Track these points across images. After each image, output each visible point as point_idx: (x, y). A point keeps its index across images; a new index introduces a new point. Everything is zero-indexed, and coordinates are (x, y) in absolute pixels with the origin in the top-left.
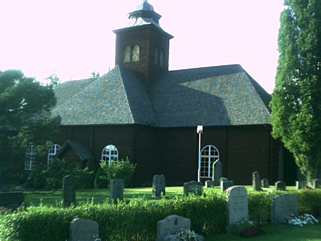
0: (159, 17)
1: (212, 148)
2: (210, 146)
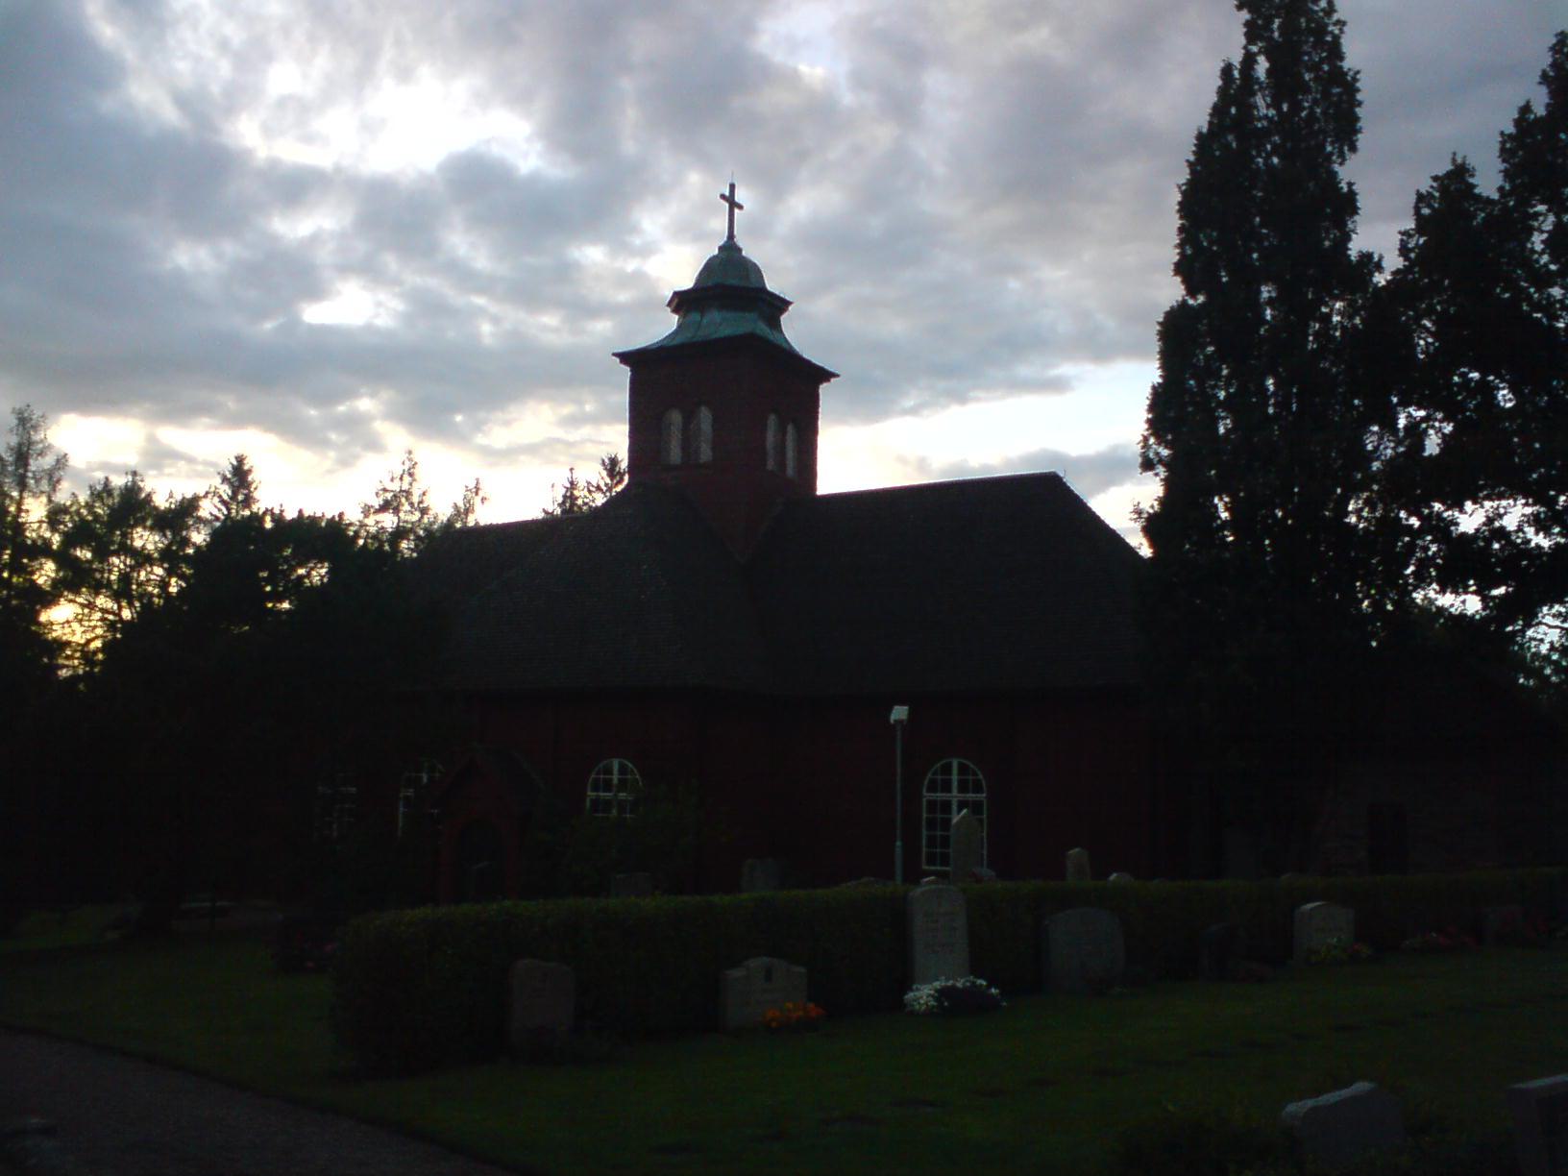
0: (780, 305)
1: (963, 769)
2: (616, 764)
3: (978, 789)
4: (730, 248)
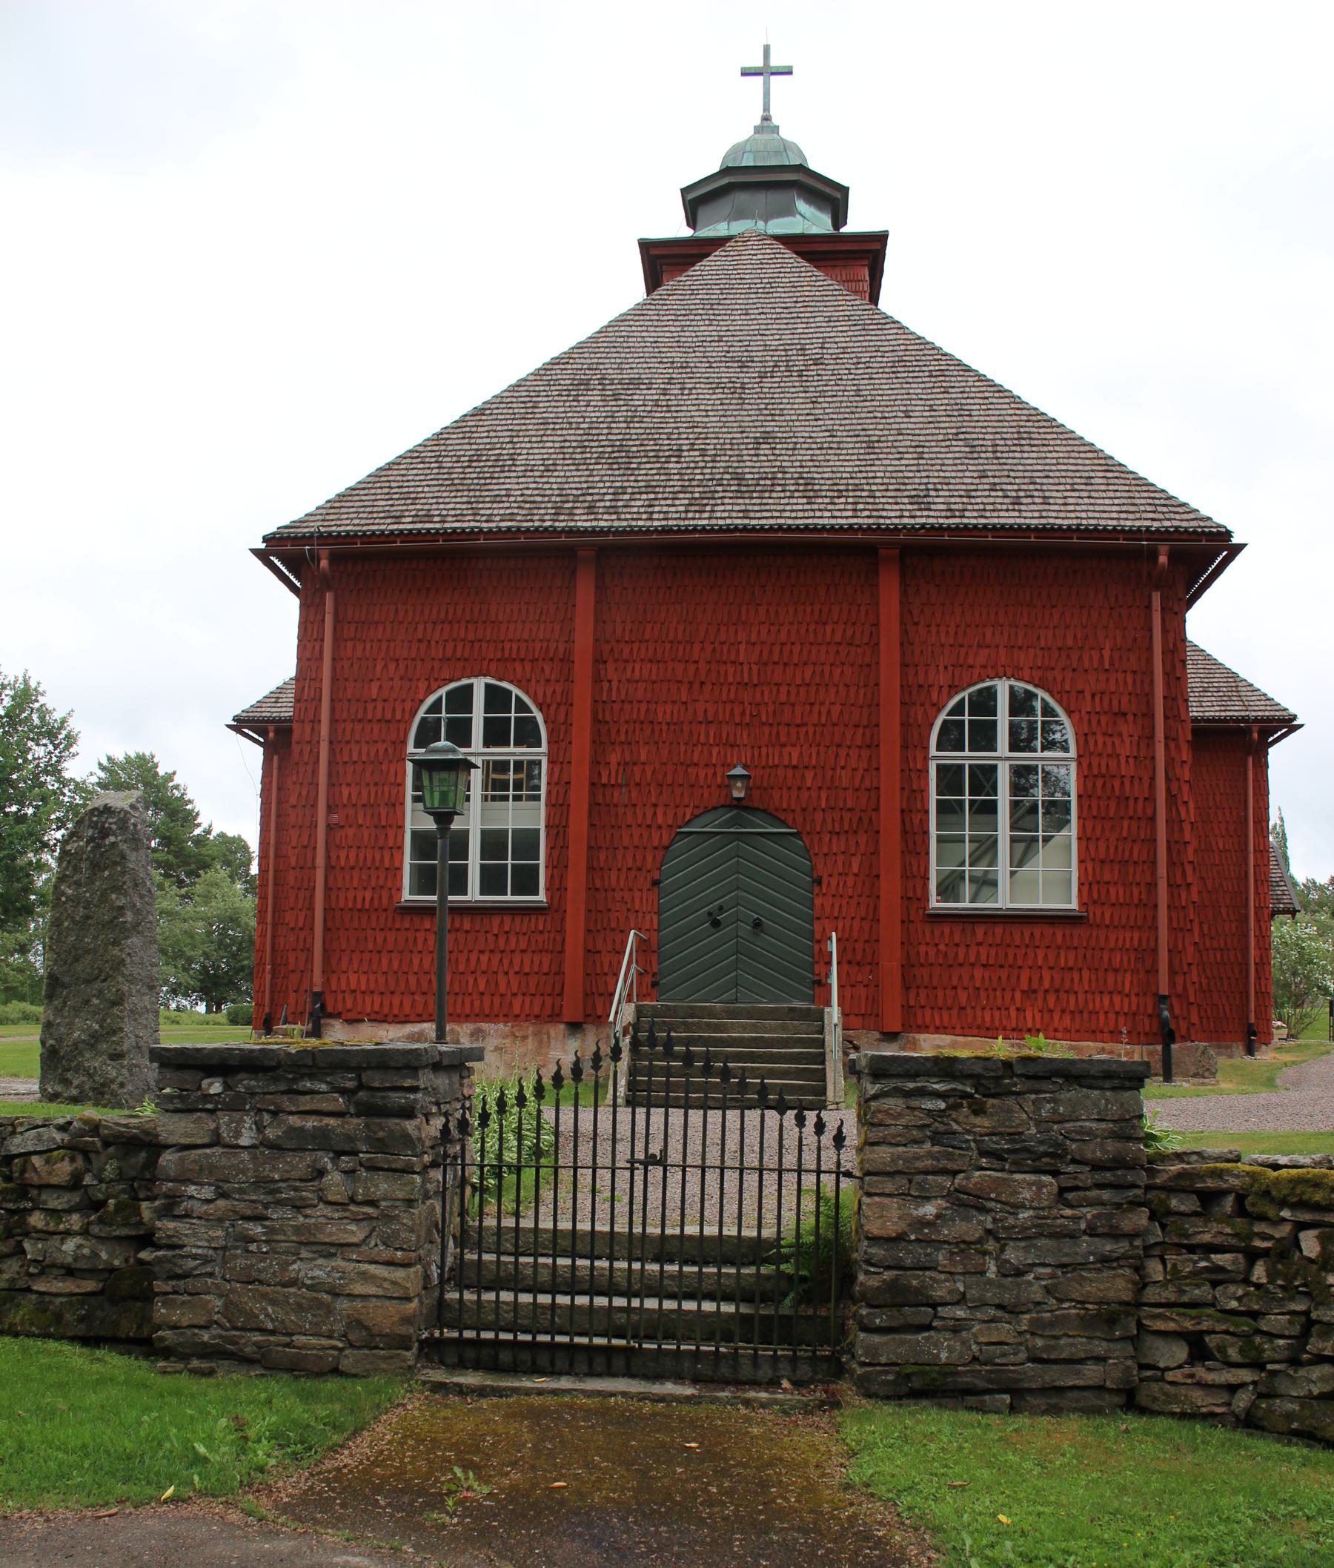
3: (527, 735)
4: (766, 125)
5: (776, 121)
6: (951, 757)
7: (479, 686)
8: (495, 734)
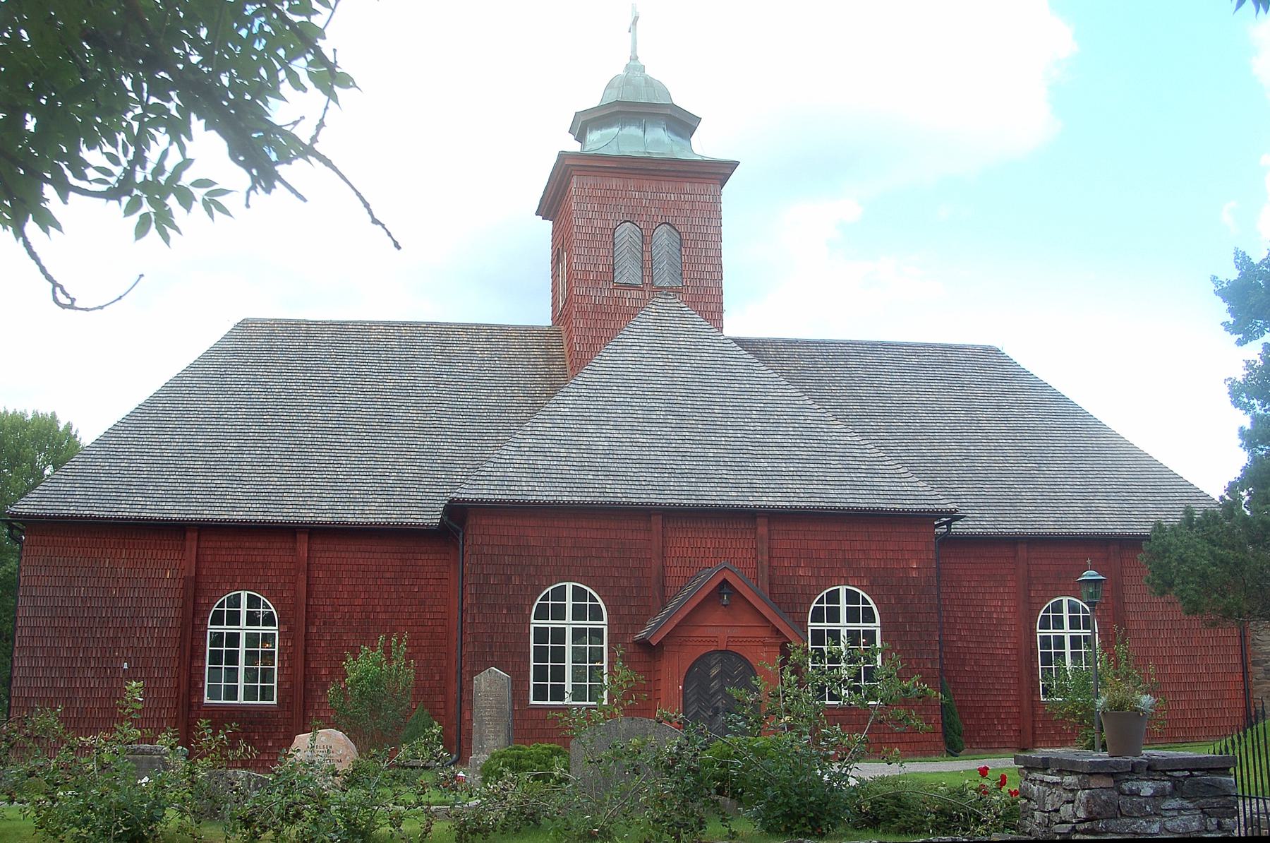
1: (579, 594)
5: (642, 60)
6: (542, 623)
7: (569, 586)
8: (578, 613)
